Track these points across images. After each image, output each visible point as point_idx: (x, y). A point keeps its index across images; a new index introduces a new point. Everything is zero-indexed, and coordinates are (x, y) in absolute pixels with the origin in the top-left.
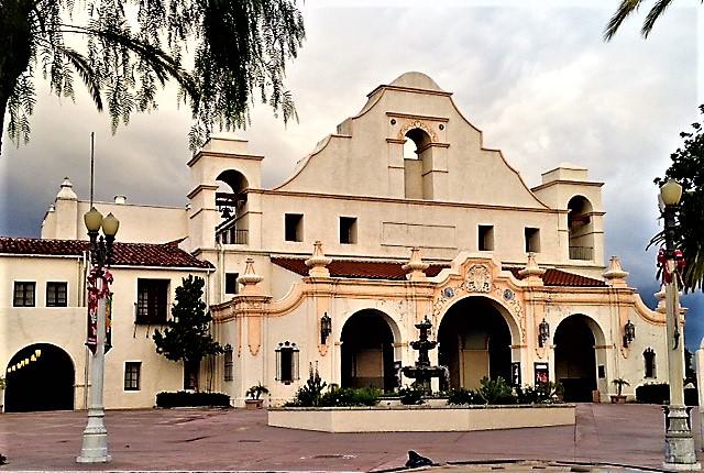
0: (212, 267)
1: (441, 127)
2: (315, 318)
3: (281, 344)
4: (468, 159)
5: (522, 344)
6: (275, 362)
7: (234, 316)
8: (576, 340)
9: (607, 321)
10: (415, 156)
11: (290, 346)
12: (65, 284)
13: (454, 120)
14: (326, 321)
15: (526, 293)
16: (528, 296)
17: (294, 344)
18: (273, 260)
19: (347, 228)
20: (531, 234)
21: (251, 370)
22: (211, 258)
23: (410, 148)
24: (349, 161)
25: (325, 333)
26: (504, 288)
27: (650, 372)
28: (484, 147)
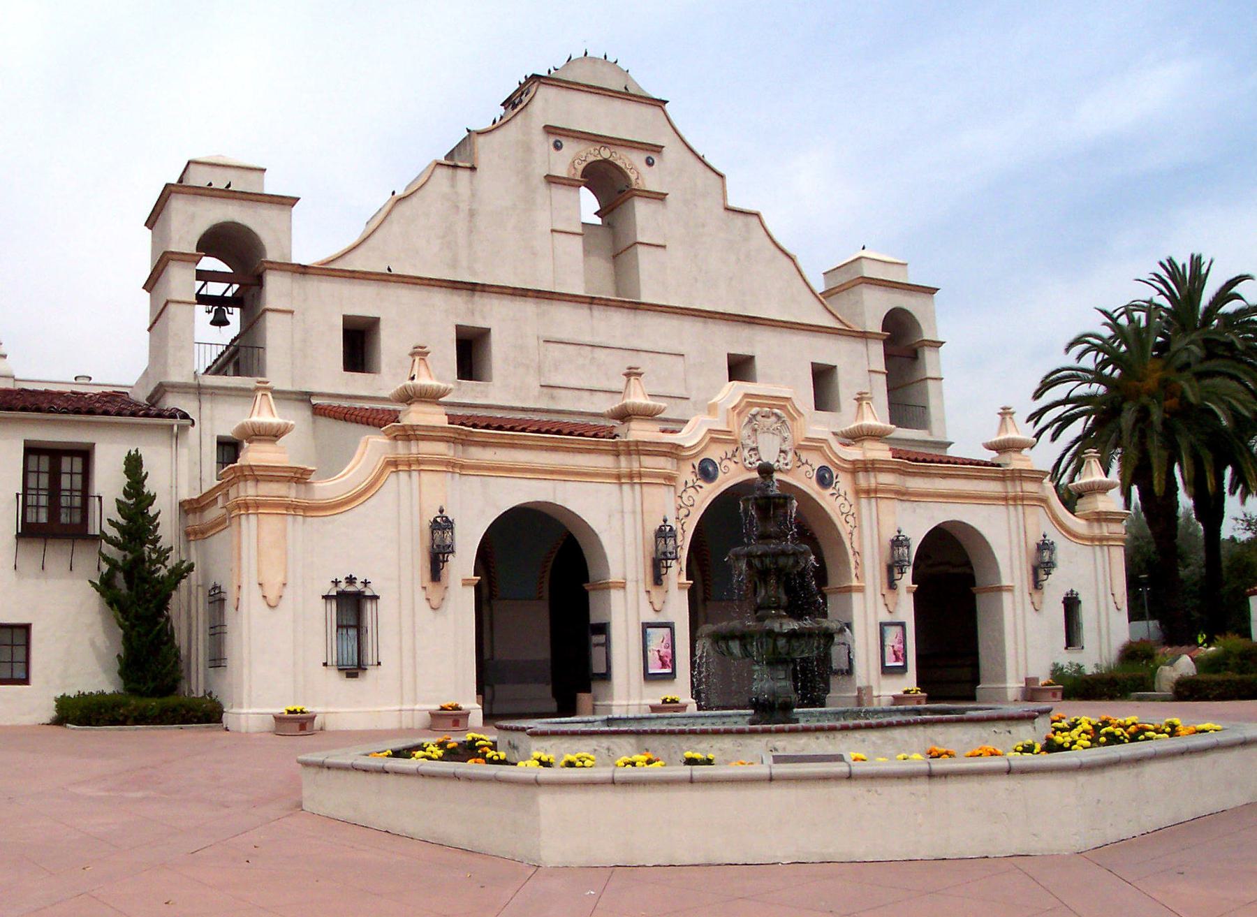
1: (650, 163)
3: (336, 583)
5: (855, 583)
7: (220, 524)
8: (949, 581)
9: (1005, 535)
11: (359, 586)
13: (672, 151)
14: (442, 525)
15: (861, 475)
16: (864, 481)
17: (366, 583)
18: (318, 411)
19: (471, 352)
20: (823, 376)
21: (270, 658)
22: (186, 404)
23: (588, 204)
24: (472, 214)
25: (438, 559)
26: (817, 462)
27: (1072, 637)
28: (732, 203)
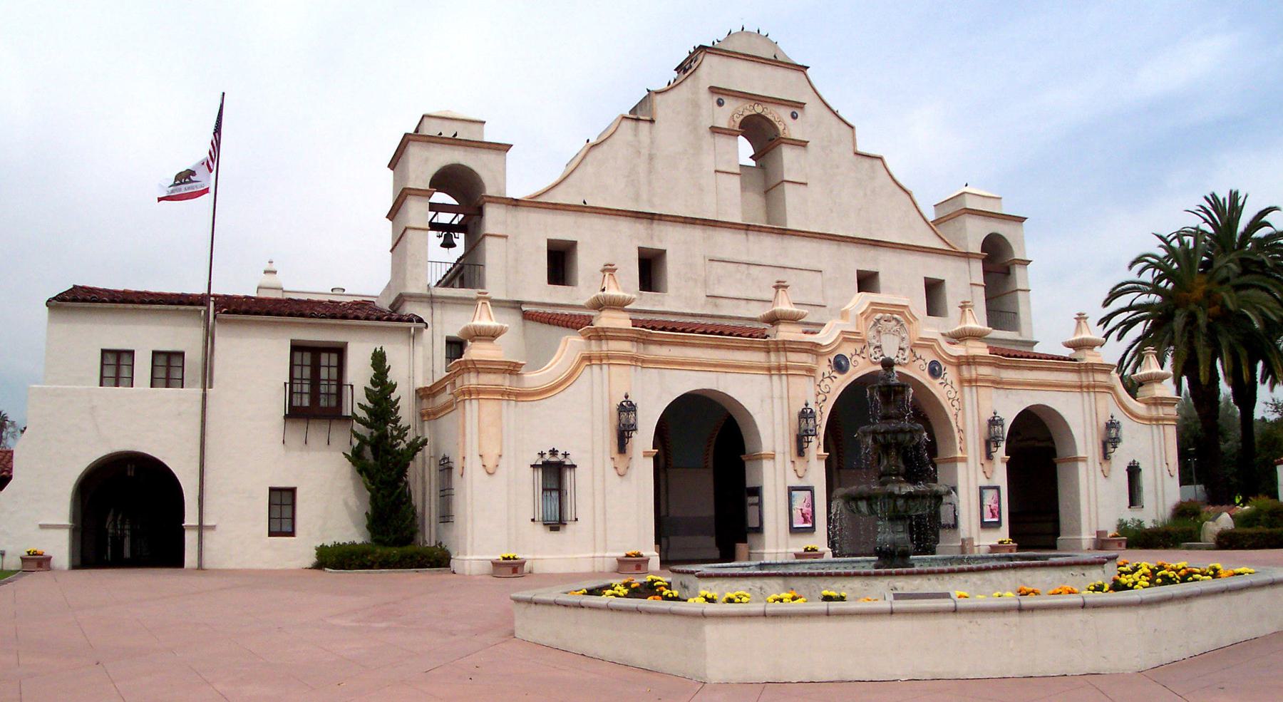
0: (420, 320)
1: (794, 116)
2: (606, 405)
3: (542, 454)
4: (838, 167)
5: (959, 455)
7: (448, 407)
8: (1035, 453)
9: (1079, 415)
11: (560, 457)
12: (182, 354)
13: (812, 107)
14: (627, 408)
16: (967, 372)
18: (527, 316)
19: (650, 269)
20: (933, 289)
22: (421, 311)
23: (744, 150)
24: (651, 158)
25: (623, 435)
26: (929, 357)
28: (860, 149)
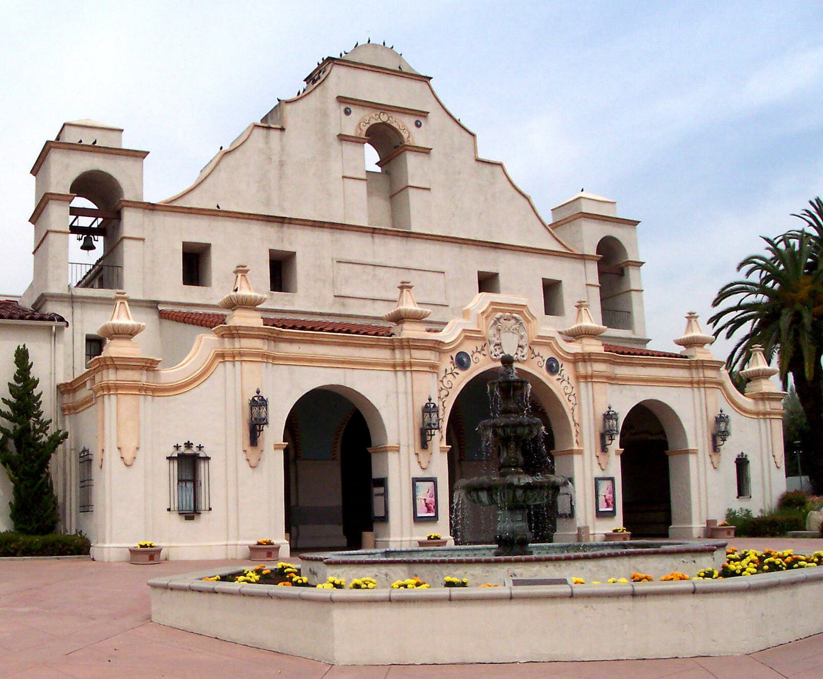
0: (61, 319)
1: (418, 125)
3: (177, 447)
5: (576, 447)
6: (164, 475)
8: (647, 445)
9: (691, 411)
10: (378, 169)
11: (194, 450)
13: (435, 115)
14: (259, 403)
15: (580, 364)
16: (582, 369)
18: (163, 315)
19: (281, 270)
22: (63, 310)
23: (370, 157)
24: (282, 164)
25: (255, 429)
26: (546, 354)
27: (743, 488)
28: (481, 156)
